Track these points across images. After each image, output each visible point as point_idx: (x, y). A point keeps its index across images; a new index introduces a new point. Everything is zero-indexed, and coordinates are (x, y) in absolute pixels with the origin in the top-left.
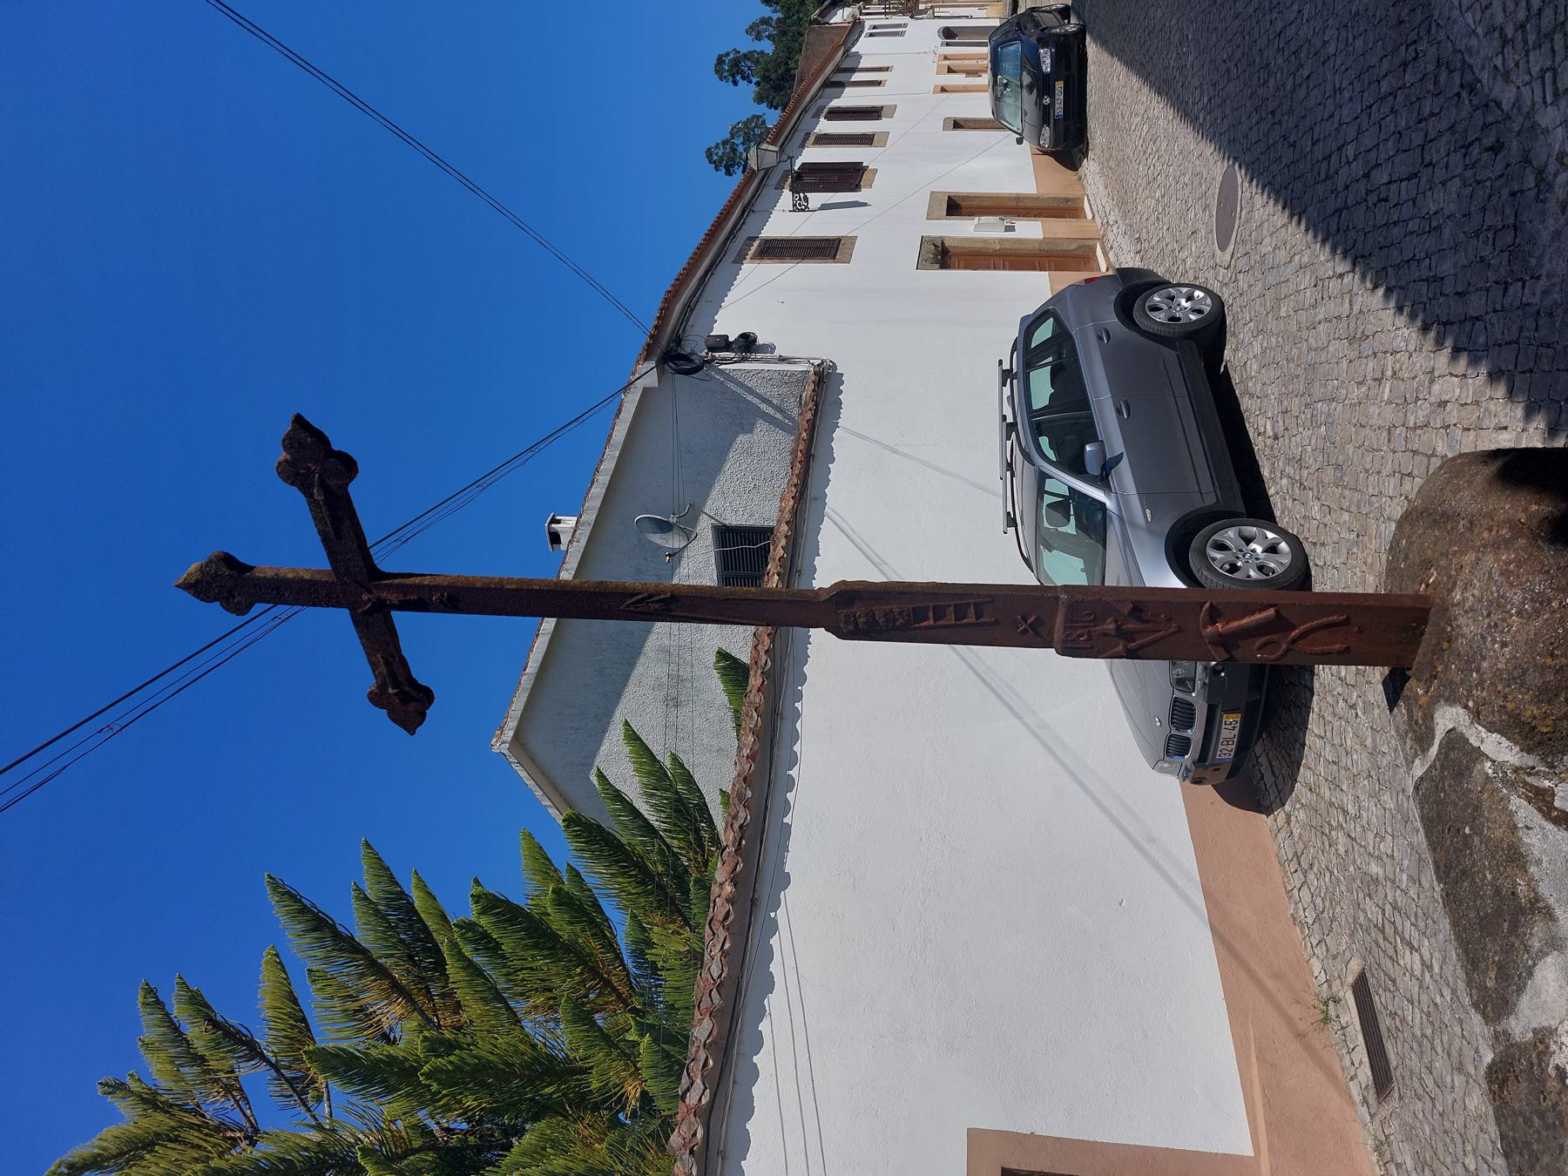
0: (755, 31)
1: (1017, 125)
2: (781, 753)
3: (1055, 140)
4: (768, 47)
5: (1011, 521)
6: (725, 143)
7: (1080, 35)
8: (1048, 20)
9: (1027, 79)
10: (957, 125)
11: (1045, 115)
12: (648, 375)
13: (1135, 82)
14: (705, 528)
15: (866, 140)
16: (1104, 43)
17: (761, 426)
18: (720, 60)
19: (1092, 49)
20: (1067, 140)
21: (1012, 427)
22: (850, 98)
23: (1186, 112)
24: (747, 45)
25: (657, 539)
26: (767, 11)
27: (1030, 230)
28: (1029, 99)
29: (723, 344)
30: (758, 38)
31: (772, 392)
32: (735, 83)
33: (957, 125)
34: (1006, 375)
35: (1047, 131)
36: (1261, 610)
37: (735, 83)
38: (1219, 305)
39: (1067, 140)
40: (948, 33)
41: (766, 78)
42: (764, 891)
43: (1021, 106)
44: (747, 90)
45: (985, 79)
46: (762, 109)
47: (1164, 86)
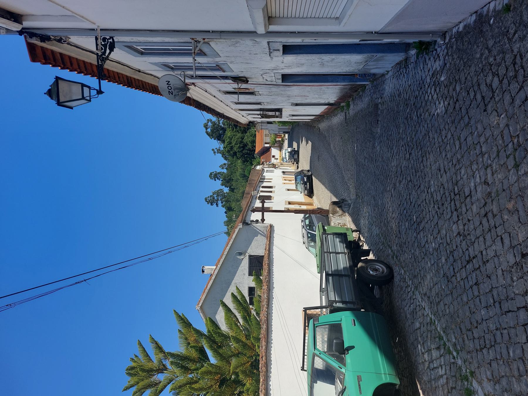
0: (222, 167)
1: (300, 190)
2: (271, 274)
3: (308, 193)
4: (225, 171)
5: (304, 243)
6: (211, 196)
7: (311, 175)
8: (305, 172)
9: (302, 182)
10: (288, 190)
11: (306, 189)
12: (240, 226)
13: (320, 183)
14: (247, 254)
15: (271, 192)
16: (315, 177)
17: (259, 235)
18: (211, 174)
19: (313, 178)
20: (310, 193)
21: (303, 227)
22: (265, 184)
23: (326, 188)
24: (219, 170)
25: (238, 257)
26: (226, 162)
27: (304, 207)
28: (303, 186)
29: (253, 221)
30: (223, 168)
31: (262, 229)
32: (215, 180)
33: (288, 190)
34: (302, 221)
35: (306, 191)
36: (266, 118)
37: (215, 180)
38: (390, 268)
39: (310, 193)
40: (284, 172)
41: (224, 179)
42: (271, 289)
43: (301, 187)
44: (219, 182)
45: (294, 182)
46: (223, 187)
47: (323, 184)
